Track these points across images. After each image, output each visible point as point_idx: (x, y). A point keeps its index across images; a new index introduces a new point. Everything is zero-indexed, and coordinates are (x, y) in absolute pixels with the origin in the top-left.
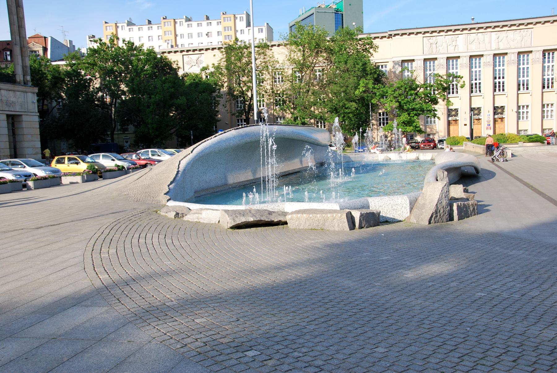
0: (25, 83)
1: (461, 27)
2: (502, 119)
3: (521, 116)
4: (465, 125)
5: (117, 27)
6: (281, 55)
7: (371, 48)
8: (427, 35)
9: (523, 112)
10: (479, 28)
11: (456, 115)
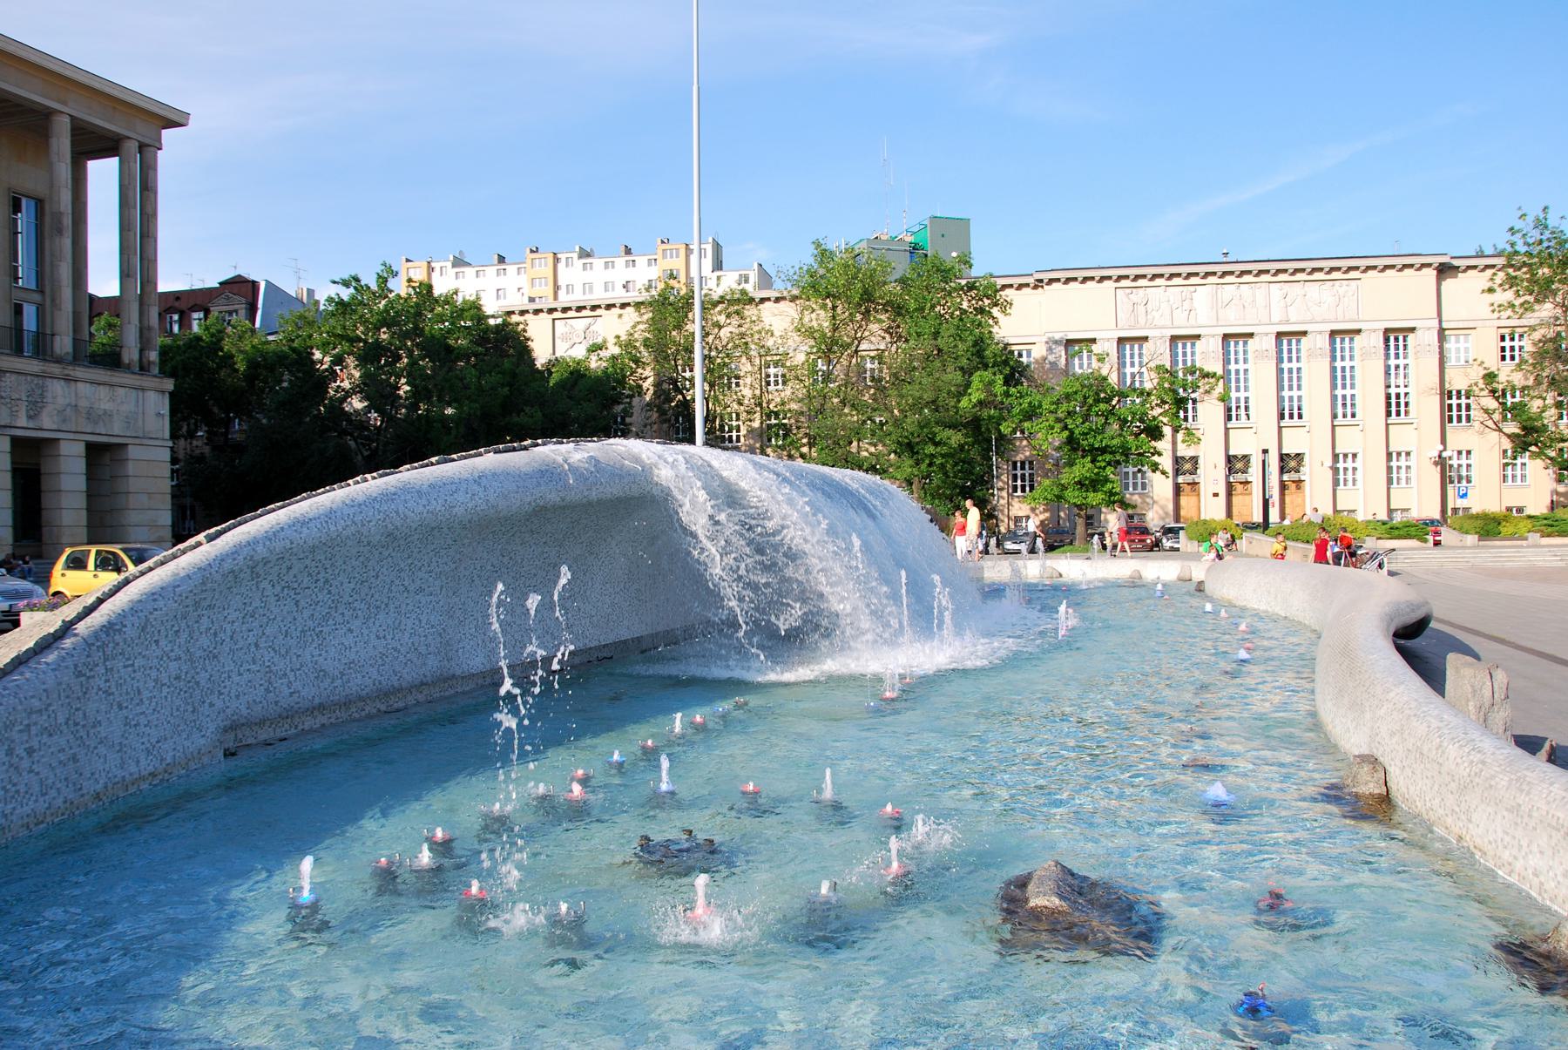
0: (144, 368)
1: (1202, 269)
2: (1299, 483)
3: (1341, 477)
4: (1216, 495)
5: (430, 269)
6: (779, 321)
7: (996, 305)
8: (1124, 283)
9: (1346, 469)
10: (1243, 273)
11: (1193, 472)
